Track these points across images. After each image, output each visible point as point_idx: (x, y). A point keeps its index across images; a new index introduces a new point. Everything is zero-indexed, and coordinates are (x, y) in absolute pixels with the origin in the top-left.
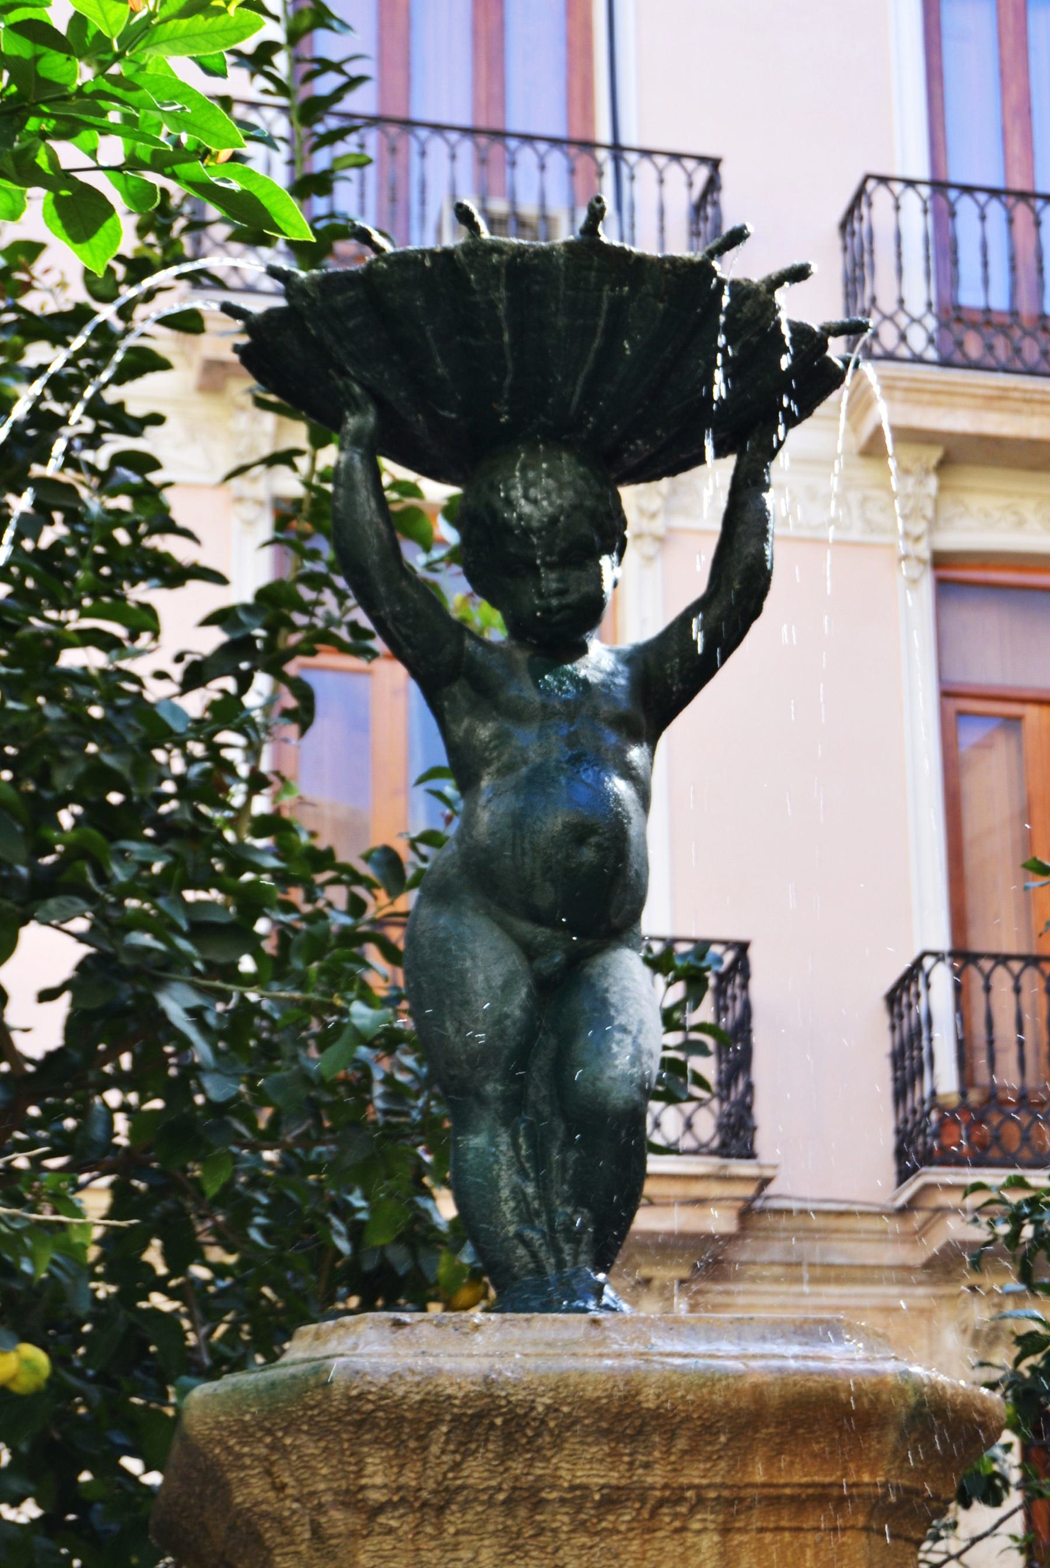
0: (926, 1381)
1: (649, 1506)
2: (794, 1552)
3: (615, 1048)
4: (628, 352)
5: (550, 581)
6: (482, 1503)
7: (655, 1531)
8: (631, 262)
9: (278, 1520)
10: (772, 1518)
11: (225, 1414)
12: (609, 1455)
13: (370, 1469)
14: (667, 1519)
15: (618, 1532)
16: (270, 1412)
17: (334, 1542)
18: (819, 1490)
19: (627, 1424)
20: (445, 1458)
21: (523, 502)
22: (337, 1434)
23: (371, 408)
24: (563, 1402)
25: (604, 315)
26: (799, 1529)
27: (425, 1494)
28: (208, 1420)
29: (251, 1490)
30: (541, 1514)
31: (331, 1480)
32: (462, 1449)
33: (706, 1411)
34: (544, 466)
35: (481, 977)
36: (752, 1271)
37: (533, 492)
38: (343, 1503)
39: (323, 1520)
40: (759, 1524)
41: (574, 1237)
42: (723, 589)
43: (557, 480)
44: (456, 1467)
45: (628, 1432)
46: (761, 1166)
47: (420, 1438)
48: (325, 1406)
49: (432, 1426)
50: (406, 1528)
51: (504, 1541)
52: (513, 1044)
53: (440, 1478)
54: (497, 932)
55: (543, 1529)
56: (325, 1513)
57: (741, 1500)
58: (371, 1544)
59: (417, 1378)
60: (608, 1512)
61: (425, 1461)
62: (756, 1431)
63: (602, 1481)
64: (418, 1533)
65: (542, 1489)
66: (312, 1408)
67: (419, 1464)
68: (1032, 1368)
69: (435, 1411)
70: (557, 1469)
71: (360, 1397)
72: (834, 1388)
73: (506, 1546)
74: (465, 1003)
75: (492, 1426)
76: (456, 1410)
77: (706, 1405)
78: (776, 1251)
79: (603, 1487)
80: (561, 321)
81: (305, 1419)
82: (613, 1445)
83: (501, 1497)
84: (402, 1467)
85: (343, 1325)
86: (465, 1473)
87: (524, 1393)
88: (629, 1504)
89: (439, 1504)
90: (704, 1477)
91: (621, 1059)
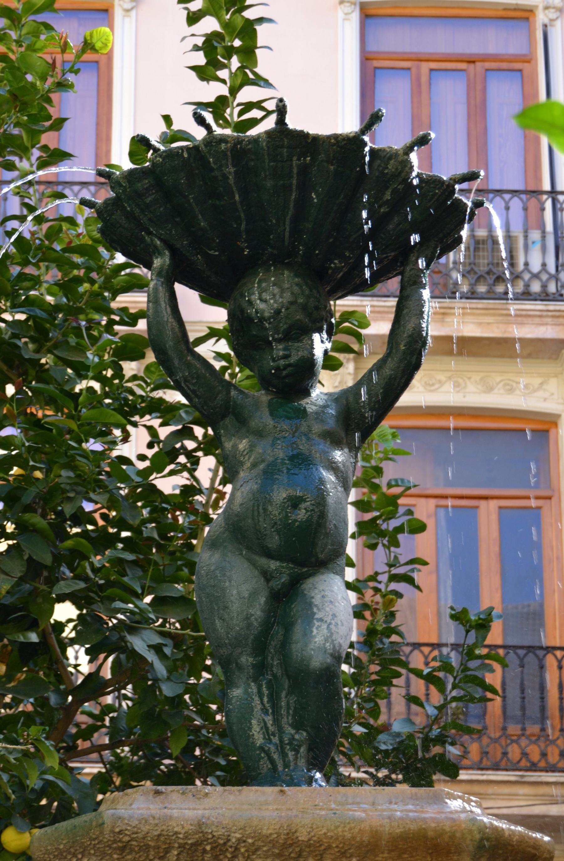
0: (488, 825)
3: (315, 631)
4: (315, 201)
5: (279, 350)
8: (310, 141)
11: (51, 845)
16: (73, 842)
19: (291, 850)
21: (258, 302)
23: (167, 253)
24: (249, 837)
25: (295, 176)
28: (42, 849)
33: (341, 842)
34: (273, 279)
35: (235, 592)
37: (265, 296)
42: (394, 351)
43: (280, 287)
45: (292, 855)
48: (101, 838)
52: (256, 632)
54: (246, 564)
59: (157, 822)
62: (377, 856)
66: (94, 839)
69: (168, 841)
71: (120, 832)
75: (205, 851)
76: (181, 841)
80: (269, 184)
81: (92, 846)
85: (127, 794)
87: (223, 831)
91: (319, 635)
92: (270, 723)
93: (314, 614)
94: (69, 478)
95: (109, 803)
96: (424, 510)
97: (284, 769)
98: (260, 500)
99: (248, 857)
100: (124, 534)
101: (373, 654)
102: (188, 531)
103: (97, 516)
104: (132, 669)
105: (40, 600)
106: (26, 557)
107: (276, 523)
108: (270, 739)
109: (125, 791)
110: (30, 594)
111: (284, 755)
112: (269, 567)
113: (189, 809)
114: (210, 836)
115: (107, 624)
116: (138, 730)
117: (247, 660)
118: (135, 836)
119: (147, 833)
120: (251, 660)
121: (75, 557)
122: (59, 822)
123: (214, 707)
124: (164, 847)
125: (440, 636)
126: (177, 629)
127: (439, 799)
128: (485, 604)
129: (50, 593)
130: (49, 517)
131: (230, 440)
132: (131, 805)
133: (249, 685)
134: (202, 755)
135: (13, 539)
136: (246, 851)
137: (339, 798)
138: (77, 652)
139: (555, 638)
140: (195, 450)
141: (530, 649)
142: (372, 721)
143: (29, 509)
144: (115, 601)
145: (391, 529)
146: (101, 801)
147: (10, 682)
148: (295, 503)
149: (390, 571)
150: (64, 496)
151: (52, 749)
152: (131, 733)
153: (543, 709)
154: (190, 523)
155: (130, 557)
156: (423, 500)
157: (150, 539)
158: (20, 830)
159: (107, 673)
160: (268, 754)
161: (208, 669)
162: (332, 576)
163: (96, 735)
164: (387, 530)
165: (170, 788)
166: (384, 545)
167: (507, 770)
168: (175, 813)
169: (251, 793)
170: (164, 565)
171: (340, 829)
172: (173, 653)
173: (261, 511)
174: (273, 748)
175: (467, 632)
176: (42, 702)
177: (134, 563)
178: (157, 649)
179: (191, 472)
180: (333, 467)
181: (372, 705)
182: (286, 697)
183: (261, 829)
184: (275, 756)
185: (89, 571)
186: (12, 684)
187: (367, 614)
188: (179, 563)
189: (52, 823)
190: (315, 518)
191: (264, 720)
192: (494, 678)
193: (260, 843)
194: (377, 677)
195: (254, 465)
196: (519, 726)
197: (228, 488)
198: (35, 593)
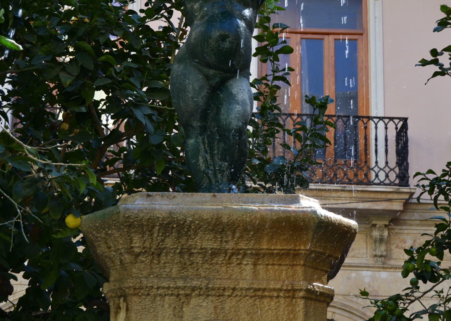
1: (228, 256)
2: (279, 272)
6: (172, 253)
7: (231, 264)
9: (110, 258)
10: (271, 261)
11: (92, 223)
12: (213, 238)
13: (135, 241)
14: (235, 260)
15: (219, 264)
16: (103, 222)
17: (126, 265)
18: (286, 251)
19: (218, 227)
20: (158, 238)
22: (123, 229)
24: (196, 220)
26: (280, 265)
27: (152, 250)
29: (102, 249)
30: (192, 257)
31: (123, 245)
32: (164, 235)
35: (191, 87)
36: (408, 222)
38: (127, 252)
39: (123, 258)
40: (267, 263)
44: (163, 241)
45: (219, 230)
46: (410, 189)
47: (150, 231)
49: (153, 227)
50: (148, 261)
51: (180, 266)
53: (157, 244)
55: (193, 262)
56: (123, 256)
57: (260, 254)
59: (148, 211)
60: (215, 257)
61: (152, 239)
63: (211, 247)
64: (152, 263)
65: (191, 249)
66: (115, 221)
67: (150, 240)
68: (442, 235)
70: (196, 242)
71: (128, 217)
73: (181, 267)
75: (173, 228)
76: (160, 222)
77: (244, 222)
78: (416, 216)
79: (212, 249)
82: (214, 235)
83: (178, 251)
86: (166, 243)
87: (183, 217)
88: (221, 255)
89: (158, 253)
90: (246, 246)
94: (102, 22)
95: (122, 201)
97: (216, 183)
98: (204, 38)
99: (196, 231)
100: (132, 53)
102: (166, 52)
104: (134, 127)
105: (87, 89)
106: (80, 65)
107: (213, 49)
108: (208, 167)
109: (132, 195)
112: (209, 73)
113: (165, 205)
114: (176, 220)
115: (123, 102)
116: (138, 161)
117: (196, 124)
118: (136, 219)
119: (143, 217)
121: (107, 66)
122: (96, 211)
123: (179, 148)
124: (151, 225)
126: (160, 105)
127: (296, 200)
129: (93, 85)
130: (92, 44)
131: (190, 3)
132: (134, 202)
133: (198, 137)
134: (172, 174)
135: (72, 56)
136: (195, 228)
138: (107, 117)
139: (363, 111)
140: (170, 7)
144: (127, 90)
145: (274, 51)
146: (119, 199)
147: (71, 134)
148: (223, 38)
149: (274, 75)
150: (100, 32)
152: (135, 162)
154: (168, 47)
155: (134, 66)
156: (294, 35)
158: (76, 216)
159: (122, 129)
160: (207, 174)
161: (176, 128)
163: (117, 163)
164: (272, 52)
166: (271, 60)
168: (157, 207)
169: (198, 196)
170: (153, 70)
171: (244, 217)
172: (157, 118)
175: (315, 109)
176: (87, 145)
178: (149, 117)
179: (168, 19)
180: (243, 18)
182: (217, 144)
183: (203, 216)
184: (211, 177)
187: (261, 98)
188: (162, 69)
189: (92, 212)
191: (205, 156)
192: (330, 134)
193: (202, 224)
194: (266, 133)
195: (202, 17)
197: (188, 29)
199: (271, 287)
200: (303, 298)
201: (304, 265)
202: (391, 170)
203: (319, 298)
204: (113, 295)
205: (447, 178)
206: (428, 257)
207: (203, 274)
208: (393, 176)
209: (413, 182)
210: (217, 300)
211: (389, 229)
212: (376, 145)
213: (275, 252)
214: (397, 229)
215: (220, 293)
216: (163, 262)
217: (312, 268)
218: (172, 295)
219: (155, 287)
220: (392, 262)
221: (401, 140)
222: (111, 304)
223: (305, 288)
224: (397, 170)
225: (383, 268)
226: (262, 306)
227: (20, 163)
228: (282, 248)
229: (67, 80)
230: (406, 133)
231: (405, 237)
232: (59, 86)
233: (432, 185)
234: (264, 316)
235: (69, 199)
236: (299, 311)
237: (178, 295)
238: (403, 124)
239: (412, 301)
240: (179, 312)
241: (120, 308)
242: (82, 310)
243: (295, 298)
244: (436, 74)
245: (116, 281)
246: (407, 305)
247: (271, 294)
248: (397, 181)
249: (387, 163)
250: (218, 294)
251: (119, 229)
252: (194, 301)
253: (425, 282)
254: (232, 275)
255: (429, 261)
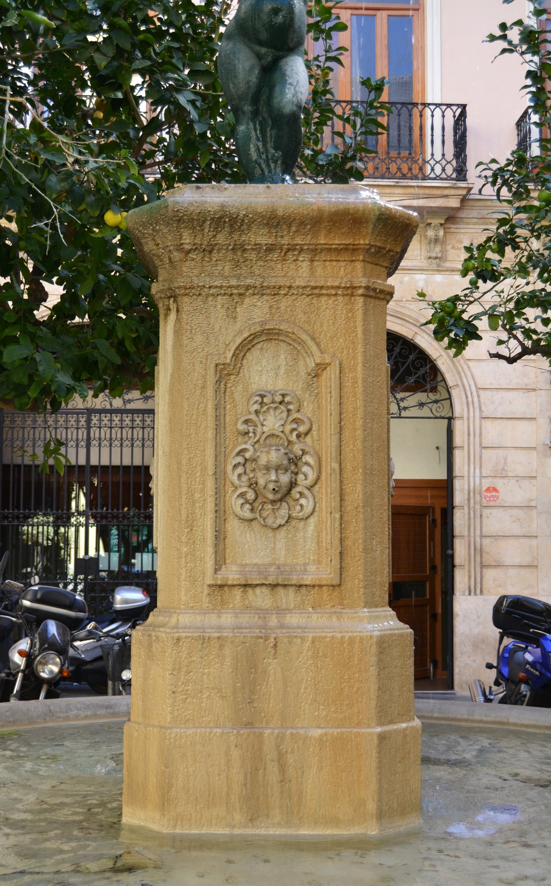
3: (287, 91)
6: (225, 250)
9: (159, 256)
13: (184, 237)
22: (172, 224)
24: (250, 213)
26: (339, 261)
27: (203, 246)
29: (149, 246)
35: (241, 67)
36: (465, 220)
41: (276, 162)
44: (214, 236)
47: (200, 226)
49: (204, 222)
57: (317, 250)
58: (187, 263)
61: (203, 235)
62: (321, 224)
68: (504, 231)
72: (349, 209)
74: (236, 76)
75: (225, 222)
78: (474, 213)
79: (266, 244)
83: (231, 247)
84: (195, 236)
91: (289, 94)
92: (261, 146)
93: (286, 80)
96: (345, 16)
100: (172, 31)
101: (316, 106)
103: (155, 19)
104: (177, 114)
105: (124, 72)
106: (115, 44)
108: (261, 157)
110: (117, 68)
111: (268, 166)
117: (247, 108)
120: (250, 108)
121: (144, 46)
125: (352, 96)
127: (356, 191)
128: (379, 76)
137: (300, 191)
141: (404, 104)
142: (315, 148)
143: (116, 15)
145: (327, 29)
148: (276, 11)
151: (134, 163)
153: (410, 141)
155: (176, 45)
156: (344, 11)
157: (188, 34)
158: (115, 213)
159: (162, 117)
162: (297, 57)
164: (325, 29)
165: (205, 185)
166: (323, 38)
167: (389, 179)
168: (208, 199)
170: (196, 51)
171: (301, 209)
173: (256, 17)
174: (262, 162)
175: (370, 92)
176: (124, 135)
177: (178, 49)
181: (315, 137)
185: (153, 54)
186: (108, 124)
190: (288, 22)
192: (383, 120)
193: (256, 217)
196: (397, 152)
198: (120, 68)
199: (329, 284)
200: (362, 295)
201: (363, 261)
202: (448, 162)
203: (378, 295)
204: (162, 296)
205: (510, 168)
206: (489, 254)
207: (257, 272)
208: (449, 170)
209: (472, 172)
210: (272, 299)
211: (444, 228)
212: (432, 135)
213: (333, 246)
214: (453, 228)
215: (275, 291)
216: (215, 259)
217: (372, 263)
218: (225, 294)
219: (207, 286)
220: (448, 265)
221: (459, 129)
222: (160, 305)
223: (364, 285)
224: (454, 163)
225: (438, 270)
226: (319, 305)
227: (53, 155)
228: (341, 242)
229: (102, 62)
230: (464, 121)
231: (462, 236)
232: (93, 69)
233: (495, 176)
234: (321, 315)
235: (108, 193)
236: (358, 309)
237: (231, 295)
238: (461, 112)
239: (471, 302)
240: (233, 312)
241: (170, 310)
242: (121, 318)
243: (354, 296)
244: (504, 51)
245: (165, 280)
246: (466, 306)
247: (329, 292)
248: (454, 176)
249: (443, 155)
250: (273, 293)
251: (168, 224)
252: (247, 301)
253: (485, 282)
254: (287, 272)
255: (490, 259)
